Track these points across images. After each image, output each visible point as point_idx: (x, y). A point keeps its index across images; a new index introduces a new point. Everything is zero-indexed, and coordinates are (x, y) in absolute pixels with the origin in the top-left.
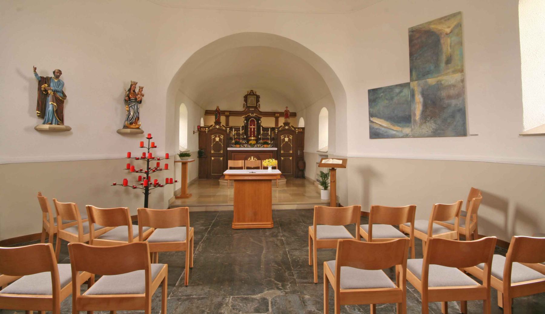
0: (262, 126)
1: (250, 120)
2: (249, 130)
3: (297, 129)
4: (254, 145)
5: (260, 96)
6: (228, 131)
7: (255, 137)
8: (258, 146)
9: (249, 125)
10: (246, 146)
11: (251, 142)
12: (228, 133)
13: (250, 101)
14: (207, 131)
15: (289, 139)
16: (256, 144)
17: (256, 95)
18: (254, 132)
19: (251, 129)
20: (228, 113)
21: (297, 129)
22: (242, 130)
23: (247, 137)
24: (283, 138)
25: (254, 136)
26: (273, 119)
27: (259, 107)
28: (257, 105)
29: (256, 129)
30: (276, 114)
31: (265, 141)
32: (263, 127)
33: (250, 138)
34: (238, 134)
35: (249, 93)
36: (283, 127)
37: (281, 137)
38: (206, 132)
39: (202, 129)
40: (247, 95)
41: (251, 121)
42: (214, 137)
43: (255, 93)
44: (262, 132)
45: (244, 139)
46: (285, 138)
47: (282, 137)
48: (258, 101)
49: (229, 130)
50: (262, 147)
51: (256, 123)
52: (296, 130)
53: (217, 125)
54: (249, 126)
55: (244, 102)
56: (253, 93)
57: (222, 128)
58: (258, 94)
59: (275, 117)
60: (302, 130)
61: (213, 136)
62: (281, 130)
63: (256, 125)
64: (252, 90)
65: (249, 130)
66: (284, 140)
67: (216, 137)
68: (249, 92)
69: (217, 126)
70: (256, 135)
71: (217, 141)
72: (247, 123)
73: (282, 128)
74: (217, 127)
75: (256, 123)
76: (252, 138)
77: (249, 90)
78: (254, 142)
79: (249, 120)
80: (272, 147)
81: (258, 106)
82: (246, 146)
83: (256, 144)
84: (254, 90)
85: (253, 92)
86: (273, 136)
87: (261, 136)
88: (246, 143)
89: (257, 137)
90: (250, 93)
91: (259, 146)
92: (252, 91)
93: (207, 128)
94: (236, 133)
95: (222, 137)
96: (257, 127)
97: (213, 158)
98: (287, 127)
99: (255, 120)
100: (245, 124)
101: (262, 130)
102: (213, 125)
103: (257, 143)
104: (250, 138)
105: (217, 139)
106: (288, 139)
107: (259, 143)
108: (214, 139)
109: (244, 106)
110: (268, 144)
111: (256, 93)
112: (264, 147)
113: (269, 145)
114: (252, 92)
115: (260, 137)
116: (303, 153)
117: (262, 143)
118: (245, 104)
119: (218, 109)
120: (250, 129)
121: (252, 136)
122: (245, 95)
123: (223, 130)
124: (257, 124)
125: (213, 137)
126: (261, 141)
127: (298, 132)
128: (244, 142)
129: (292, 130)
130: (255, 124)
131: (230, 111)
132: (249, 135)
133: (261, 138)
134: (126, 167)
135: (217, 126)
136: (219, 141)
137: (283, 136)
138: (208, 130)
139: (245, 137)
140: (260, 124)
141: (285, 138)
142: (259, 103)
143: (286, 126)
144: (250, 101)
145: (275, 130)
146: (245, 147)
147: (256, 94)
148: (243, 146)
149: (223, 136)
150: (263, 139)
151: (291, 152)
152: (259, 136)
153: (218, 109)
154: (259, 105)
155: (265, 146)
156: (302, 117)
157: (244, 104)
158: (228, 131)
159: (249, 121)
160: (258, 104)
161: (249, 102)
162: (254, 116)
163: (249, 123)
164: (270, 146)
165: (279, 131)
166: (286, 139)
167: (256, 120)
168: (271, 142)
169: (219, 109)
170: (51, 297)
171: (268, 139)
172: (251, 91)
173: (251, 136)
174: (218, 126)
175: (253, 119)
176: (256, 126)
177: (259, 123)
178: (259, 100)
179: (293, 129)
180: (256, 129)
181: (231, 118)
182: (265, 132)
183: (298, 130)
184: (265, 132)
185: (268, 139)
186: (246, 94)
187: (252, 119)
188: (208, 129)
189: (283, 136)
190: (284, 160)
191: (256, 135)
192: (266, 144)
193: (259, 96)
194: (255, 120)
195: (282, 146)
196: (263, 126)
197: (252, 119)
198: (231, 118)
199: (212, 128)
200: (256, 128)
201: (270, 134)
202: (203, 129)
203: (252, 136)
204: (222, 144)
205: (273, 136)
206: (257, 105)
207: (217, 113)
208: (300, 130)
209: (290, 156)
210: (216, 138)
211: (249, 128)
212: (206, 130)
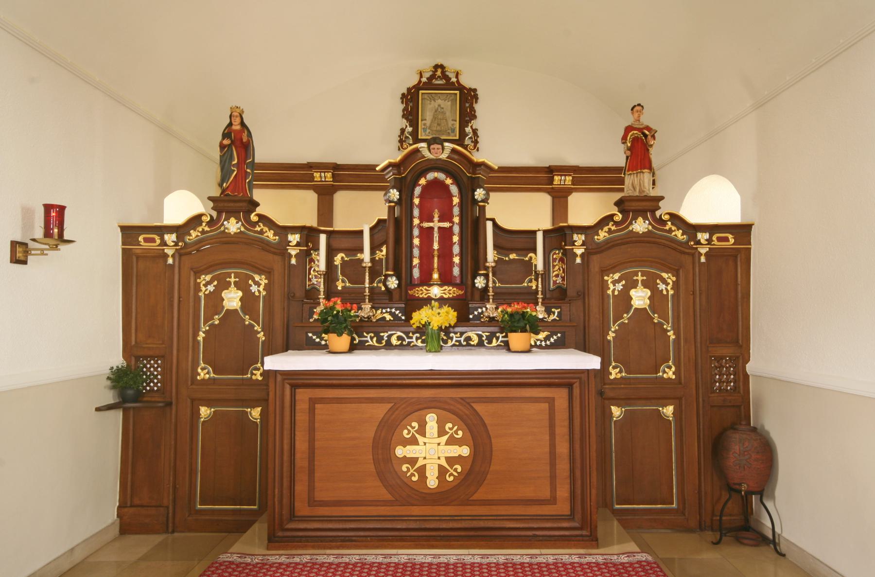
0: (493, 220)
1: (423, 181)
2: (416, 241)
3: (703, 237)
4: (447, 330)
5: (480, 93)
6: (293, 252)
7: (454, 285)
8: (468, 339)
9: (416, 212)
10: (394, 341)
11: (420, 316)
12: (293, 261)
13: (429, 116)
14: (170, 252)
15: (656, 297)
16: (456, 326)
17: (461, 88)
18: (446, 254)
19: (427, 234)
20: (329, 175)
21: (706, 236)
22: (374, 249)
23: (406, 283)
24: (619, 287)
25: (446, 280)
26: (544, 202)
27: (476, 142)
28: (463, 134)
29: (456, 239)
30: (556, 178)
31: (516, 307)
32: (495, 225)
33: (421, 292)
34: (353, 269)
35: (424, 80)
36: (616, 224)
37: (604, 286)
38: (166, 256)
39: (141, 239)
40: (418, 87)
41: (425, 188)
42: (211, 288)
43: (454, 80)
44: (491, 255)
45: (380, 298)
46: (633, 293)
47: (614, 285)
48: (467, 115)
49: (298, 244)
50: (494, 343)
51: (456, 200)
52: (698, 243)
53: (227, 219)
54: (416, 221)
55: (404, 123)
56: (445, 76)
57: (262, 232)
58: (467, 81)
59: (551, 192)
60: (732, 241)
61: (208, 278)
62: (607, 242)
63: (456, 211)
64: (439, 61)
65: (416, 241)
66: (624, 299)
67: (227, 286)
68: (428, 75)
69: (233, 220)
70: (456, 271)
71: (231, 313)
72: (405, 202)
73: (610, 231)
74: (233, 226)
75: (456, 200)
76: (436, 291)
77: (426, 64)
78: (448, 316)
79: (415, 184)
80: (559, 345)
81: (467, 141)
82: (399, 338)
83: (456, 326)
84: (452, 65)
85: (443, 73)
86: (557, 276)
87: (486, 276)
88: (395, 323)
89: (465, 282)
90: (430, 79)
91: (475, 340)
92: (442, 67)
93: (173, 237)
94: (344, 262)
95: (259, 285)
96: (461, 224)
97: (205, 412)
98: (640, 226)
99: (449, 181)
100: (391, 210)
101: (496, 247)
102: (206, 219)
103: (463, 319)
104: (421, 292)
105: (232, 299)
106: (649, 293)
107: (479, 323)
108: (215, 299)
109: (401, 141)
110: (533, 325)
111: (457, 77)
112: (506, 346)
113: (537, 333)
114: (439, 73)
115: (480, 282)
116: (746, 377)
117: (492, 319)
118: (410, 129)
119: (236, 127)
120: (420, 236)
121: (436, 276)
122: (409, 90)
123: (265, 245)
124: (461, 205)
125: (206, 285)
126: (490, 309)
127: (707, 255)
128: (388, 317)
129: (674, 241)
130: (451, 207)
131: (335, 168)
132: (416, 273)
133: (485, 289)
134: (110, 368)
135: (233, 220)
136: (242, 307)
137: (208, 278)
138: (176, 244)
139: (393, 283)
140: (483, 209)
141: (633, 293)
142: (475, 124)
143: (635, 218)
144: (429, 116)
145: (573, 243)
146: (389, 346)
147: (458, 81)
148: (379, 340)
149: (264, 282)
150: (501, 297)
151: (670, 374)
152: (474, 278)
153: (236, 127)
154: (475, 132)
155: (517, 339)
156: (253, 380)
157: (403, 131)
158: (293, 252)
159: (418, 191)
160: (468, 130)
161: (428, 122)
162: (444, 156)
163: (416, 201)
164: (547, 338)
165: (592, 250)
166: (640, 298)
167: (457, 182)
168: (549, 312)
169: (242, 124)
170: (316, 405)
171: (530, 297)
172: (437, 67)
173: (426, 280)
174: (238, 220)
175: (441, 176)
176: (456, 220)
177: (475, 202)
178: (473, 109)
179: (679, 234)
180: (456, 239)
181: (341, 199)
182: (513, 256)
183: (709, 241)
184: (513, 256)
185: (530, 297)
186: (414, 81)
187: (431, 176)
188: (180, 238)
189: (616, 276)
190: (629, 418)
191: (456, 271)
192: (524, 330)
193: (475, 90)
194: (449, 181)
195: (611, 336)
196: (500, 223)
197: (431, 176)
198: (341, 199)
199: (203, 232)
200: (456, 229)
201: (540, 267)
202: (146, 240)
203: (436, 276)
204: (257, 328)
205: (557, 276)
206: (463, 134)
207: (229, 146)
208: (719, 239)
209: (664, 400)
210: (225, 294)
211: (416, 232)
212: (164, 243)
